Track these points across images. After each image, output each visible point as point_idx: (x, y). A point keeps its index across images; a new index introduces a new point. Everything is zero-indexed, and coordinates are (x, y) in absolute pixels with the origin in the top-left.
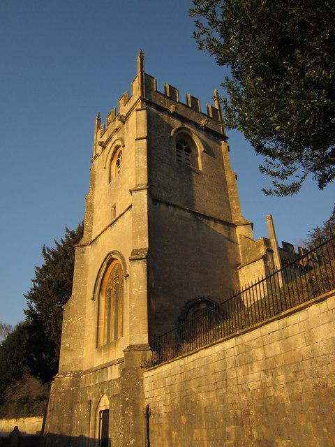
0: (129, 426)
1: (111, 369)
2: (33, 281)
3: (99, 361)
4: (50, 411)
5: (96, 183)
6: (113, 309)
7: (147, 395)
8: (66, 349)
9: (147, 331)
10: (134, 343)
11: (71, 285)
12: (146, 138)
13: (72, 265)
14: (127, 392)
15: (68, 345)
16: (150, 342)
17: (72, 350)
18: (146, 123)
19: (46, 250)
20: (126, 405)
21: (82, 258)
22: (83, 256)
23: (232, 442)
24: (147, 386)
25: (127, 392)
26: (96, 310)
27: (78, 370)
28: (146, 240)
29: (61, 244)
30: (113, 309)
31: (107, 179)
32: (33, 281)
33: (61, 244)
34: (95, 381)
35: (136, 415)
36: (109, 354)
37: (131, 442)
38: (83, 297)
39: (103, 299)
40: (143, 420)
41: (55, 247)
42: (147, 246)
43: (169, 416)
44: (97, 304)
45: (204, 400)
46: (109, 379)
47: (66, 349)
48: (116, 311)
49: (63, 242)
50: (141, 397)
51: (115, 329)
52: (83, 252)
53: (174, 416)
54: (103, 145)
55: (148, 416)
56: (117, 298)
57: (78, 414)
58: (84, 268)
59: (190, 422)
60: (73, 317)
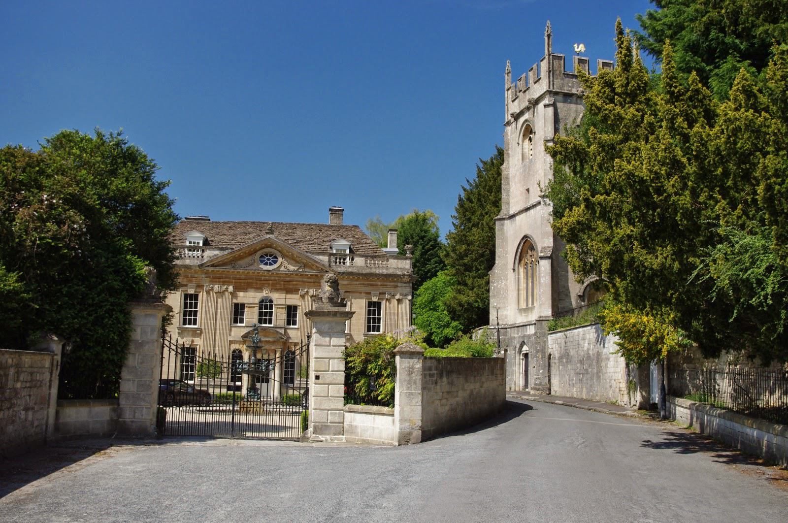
3: (521, 320)
5: (510, 152)
6: (530, 280)
7: (550, 347)
9: (551, 307)
10: (542, 315)
11: (495, 251)
12: (550, 258)
13: (494, 246)
16: (552, 315)
18: (553, 121)
20: (538, 351)
21: (503, 234)
22: (503, 228)
23: (678, 218)
24: (550, 342)
26: (525, 324)
28: (551, 240)
30: (530, 280)
31: (520, 157)
34: (518, 334)
36: (527, 316)
37: (541, 372)
38: (505, 265)
39: (522, 270)
42: (552, 245)
43: (559, 358)
44: (517, 274)
45: (572, 352)
48: (532, 282)
50: (546, 347)
51: (530, 294)
52: (503, 225)
53: (561, 358)
54: (516, 117)
55: (549, 359)
56: (533, 271)
58: (505, 240)
59: (567, 362)
60: (498, 282)
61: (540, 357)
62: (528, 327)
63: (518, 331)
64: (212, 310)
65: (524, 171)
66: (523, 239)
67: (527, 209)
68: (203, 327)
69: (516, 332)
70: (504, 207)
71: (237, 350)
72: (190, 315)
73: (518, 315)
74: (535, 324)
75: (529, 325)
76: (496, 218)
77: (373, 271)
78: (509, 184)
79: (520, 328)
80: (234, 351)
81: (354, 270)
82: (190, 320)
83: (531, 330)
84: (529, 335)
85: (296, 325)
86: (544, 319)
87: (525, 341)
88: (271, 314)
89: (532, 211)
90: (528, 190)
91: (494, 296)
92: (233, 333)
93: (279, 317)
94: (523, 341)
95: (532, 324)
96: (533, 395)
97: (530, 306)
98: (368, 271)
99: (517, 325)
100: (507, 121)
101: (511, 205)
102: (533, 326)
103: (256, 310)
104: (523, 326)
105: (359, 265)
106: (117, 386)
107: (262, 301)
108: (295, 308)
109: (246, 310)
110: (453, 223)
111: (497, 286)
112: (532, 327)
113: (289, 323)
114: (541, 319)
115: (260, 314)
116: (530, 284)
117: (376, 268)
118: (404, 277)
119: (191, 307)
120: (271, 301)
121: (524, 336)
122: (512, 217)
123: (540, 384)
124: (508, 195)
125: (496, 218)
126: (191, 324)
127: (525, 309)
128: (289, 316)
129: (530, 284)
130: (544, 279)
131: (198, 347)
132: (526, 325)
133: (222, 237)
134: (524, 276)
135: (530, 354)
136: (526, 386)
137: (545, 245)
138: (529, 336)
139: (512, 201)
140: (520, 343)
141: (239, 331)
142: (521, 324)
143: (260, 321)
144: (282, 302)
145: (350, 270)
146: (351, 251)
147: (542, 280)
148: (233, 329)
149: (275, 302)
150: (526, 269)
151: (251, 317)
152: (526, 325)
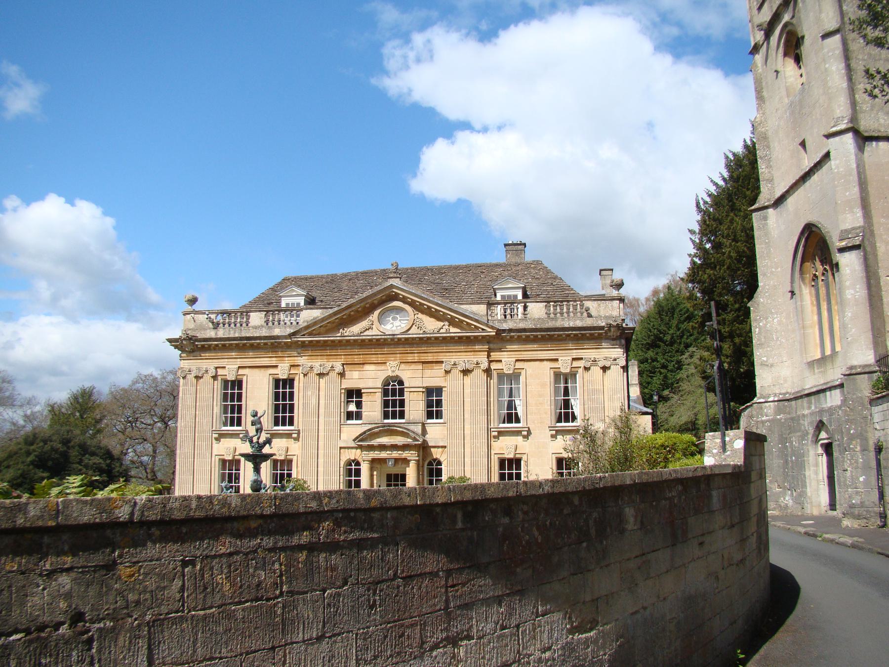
0: (857, 462)
1: (831, 394)
2: (690, 255)
4: (807, 433)
8: (764, 275)
9: (871, 346)
14: (851, 423)
15: (765, 359)
17: (772, 366)
19: (701, 202)
22: (766, 224)
25: (851, 423)
27: (784, 391)
29: (721, 183)
32: (690, 255)
33: (721, 183)
34: (809, 408)
35: (864, 449)
36: (824, 372)
37: (861, 479)
40: (872, 454)
41: (713, 189)
46: (829, 405)
47: (763, 364)
48: (829, 310)
49: (724, 179)
52: (765, 218)
57: (792, 449)
61: (858, 448)
62: (828, 393)
63: (810, 403)
64: (314, 401)
65: (792, 113)
66: (802, 233)
67: (806, 177)
68: (301, 428)
69: (805, 404)
70: (764, 188)
71: (353, 461)
72: (284, 411)
73: (807, 373)
74: (841, 386)
75: (830, 389)
76: (753, 207)
77: (559, 324)
78: (768, 147)
79: (813, 398)
80: (349, 463)
81: (530, 325)
82: (284, 418)
83: (834, 399)
84: (830, 408)
85: (441, 418)
86: (859, 370)
87: (825, 420)
88: (402, 403)
89: (815, 178)
90: (803, 144)
91: (761, 345)
92: (343, 436)
93: (415, 406)
94: (821, 422)
95: (835, 387)
96: (849, 532)
97: (828, 352)
98: (551, 324)
99: (806, 392)
100: (753, 44)
101: (776, 181)
102: (838, 391)
103: (378, 398)
104: (818, 392)
105: (537, 316)
106: (438, 510)
107: (386, 383)
108: (439, 391)
109: (364, 399)
110: (691, 239)
111: (765, 325)
112: (837, 393)
113: (430, 415)
114: (854, 371)
115: (386, 404)
116: (825, 314)
117: (563, 320)
118: (609, 330)
119: (284, 399)
120: (401, 383)
121: (821, 411)
122: (779, 202)
123: (862, 505)
124: (769, 167)
125: (753, 207)
126: (286, 426)
127: (818, 360)
128: (429, 404)
129: (825, 314)
130: (852, 292)
131: (295, 458)
132: (823, 391)
133: (337, 294)
134: (812, 303)
135: (835, 444)
136: (832, 506)
137: (847, 226)
138: (831, 411)
139: (776, 174)
140: (815, 424)
141: (354, 429)
142: (814, 390)
143: (386, 416)
144: (418, 383)
145: (522, 325)
146: (525, 295)
147: (849, 294)
148: (344, 428)
149: (406, 385)
150: (816, 287)
151: (373, 409)
152: (823, 391)
